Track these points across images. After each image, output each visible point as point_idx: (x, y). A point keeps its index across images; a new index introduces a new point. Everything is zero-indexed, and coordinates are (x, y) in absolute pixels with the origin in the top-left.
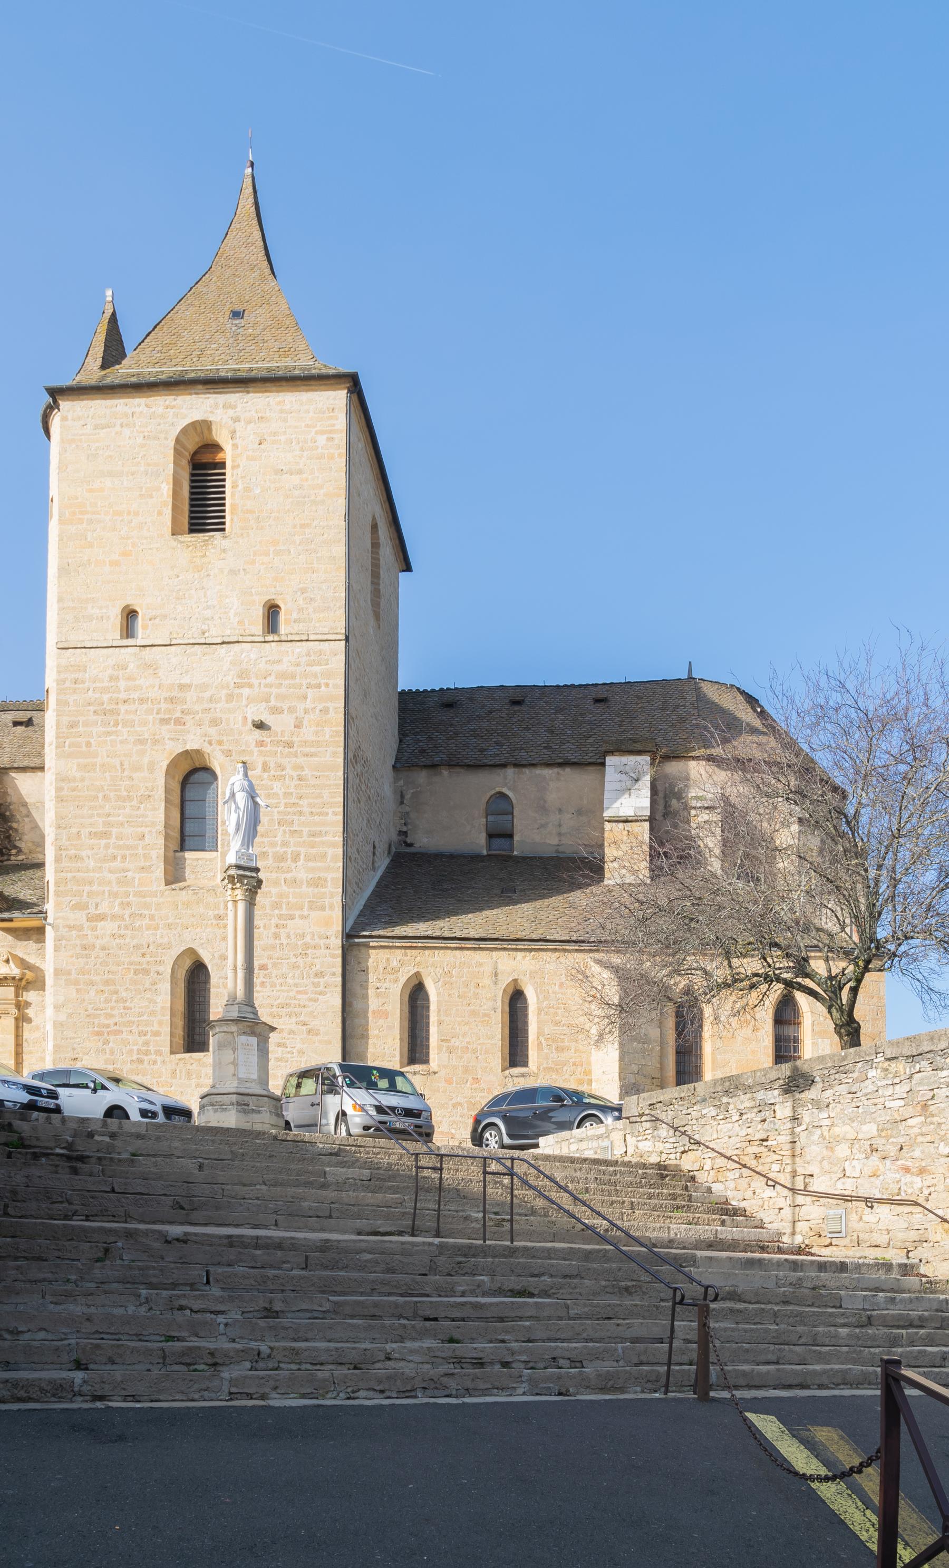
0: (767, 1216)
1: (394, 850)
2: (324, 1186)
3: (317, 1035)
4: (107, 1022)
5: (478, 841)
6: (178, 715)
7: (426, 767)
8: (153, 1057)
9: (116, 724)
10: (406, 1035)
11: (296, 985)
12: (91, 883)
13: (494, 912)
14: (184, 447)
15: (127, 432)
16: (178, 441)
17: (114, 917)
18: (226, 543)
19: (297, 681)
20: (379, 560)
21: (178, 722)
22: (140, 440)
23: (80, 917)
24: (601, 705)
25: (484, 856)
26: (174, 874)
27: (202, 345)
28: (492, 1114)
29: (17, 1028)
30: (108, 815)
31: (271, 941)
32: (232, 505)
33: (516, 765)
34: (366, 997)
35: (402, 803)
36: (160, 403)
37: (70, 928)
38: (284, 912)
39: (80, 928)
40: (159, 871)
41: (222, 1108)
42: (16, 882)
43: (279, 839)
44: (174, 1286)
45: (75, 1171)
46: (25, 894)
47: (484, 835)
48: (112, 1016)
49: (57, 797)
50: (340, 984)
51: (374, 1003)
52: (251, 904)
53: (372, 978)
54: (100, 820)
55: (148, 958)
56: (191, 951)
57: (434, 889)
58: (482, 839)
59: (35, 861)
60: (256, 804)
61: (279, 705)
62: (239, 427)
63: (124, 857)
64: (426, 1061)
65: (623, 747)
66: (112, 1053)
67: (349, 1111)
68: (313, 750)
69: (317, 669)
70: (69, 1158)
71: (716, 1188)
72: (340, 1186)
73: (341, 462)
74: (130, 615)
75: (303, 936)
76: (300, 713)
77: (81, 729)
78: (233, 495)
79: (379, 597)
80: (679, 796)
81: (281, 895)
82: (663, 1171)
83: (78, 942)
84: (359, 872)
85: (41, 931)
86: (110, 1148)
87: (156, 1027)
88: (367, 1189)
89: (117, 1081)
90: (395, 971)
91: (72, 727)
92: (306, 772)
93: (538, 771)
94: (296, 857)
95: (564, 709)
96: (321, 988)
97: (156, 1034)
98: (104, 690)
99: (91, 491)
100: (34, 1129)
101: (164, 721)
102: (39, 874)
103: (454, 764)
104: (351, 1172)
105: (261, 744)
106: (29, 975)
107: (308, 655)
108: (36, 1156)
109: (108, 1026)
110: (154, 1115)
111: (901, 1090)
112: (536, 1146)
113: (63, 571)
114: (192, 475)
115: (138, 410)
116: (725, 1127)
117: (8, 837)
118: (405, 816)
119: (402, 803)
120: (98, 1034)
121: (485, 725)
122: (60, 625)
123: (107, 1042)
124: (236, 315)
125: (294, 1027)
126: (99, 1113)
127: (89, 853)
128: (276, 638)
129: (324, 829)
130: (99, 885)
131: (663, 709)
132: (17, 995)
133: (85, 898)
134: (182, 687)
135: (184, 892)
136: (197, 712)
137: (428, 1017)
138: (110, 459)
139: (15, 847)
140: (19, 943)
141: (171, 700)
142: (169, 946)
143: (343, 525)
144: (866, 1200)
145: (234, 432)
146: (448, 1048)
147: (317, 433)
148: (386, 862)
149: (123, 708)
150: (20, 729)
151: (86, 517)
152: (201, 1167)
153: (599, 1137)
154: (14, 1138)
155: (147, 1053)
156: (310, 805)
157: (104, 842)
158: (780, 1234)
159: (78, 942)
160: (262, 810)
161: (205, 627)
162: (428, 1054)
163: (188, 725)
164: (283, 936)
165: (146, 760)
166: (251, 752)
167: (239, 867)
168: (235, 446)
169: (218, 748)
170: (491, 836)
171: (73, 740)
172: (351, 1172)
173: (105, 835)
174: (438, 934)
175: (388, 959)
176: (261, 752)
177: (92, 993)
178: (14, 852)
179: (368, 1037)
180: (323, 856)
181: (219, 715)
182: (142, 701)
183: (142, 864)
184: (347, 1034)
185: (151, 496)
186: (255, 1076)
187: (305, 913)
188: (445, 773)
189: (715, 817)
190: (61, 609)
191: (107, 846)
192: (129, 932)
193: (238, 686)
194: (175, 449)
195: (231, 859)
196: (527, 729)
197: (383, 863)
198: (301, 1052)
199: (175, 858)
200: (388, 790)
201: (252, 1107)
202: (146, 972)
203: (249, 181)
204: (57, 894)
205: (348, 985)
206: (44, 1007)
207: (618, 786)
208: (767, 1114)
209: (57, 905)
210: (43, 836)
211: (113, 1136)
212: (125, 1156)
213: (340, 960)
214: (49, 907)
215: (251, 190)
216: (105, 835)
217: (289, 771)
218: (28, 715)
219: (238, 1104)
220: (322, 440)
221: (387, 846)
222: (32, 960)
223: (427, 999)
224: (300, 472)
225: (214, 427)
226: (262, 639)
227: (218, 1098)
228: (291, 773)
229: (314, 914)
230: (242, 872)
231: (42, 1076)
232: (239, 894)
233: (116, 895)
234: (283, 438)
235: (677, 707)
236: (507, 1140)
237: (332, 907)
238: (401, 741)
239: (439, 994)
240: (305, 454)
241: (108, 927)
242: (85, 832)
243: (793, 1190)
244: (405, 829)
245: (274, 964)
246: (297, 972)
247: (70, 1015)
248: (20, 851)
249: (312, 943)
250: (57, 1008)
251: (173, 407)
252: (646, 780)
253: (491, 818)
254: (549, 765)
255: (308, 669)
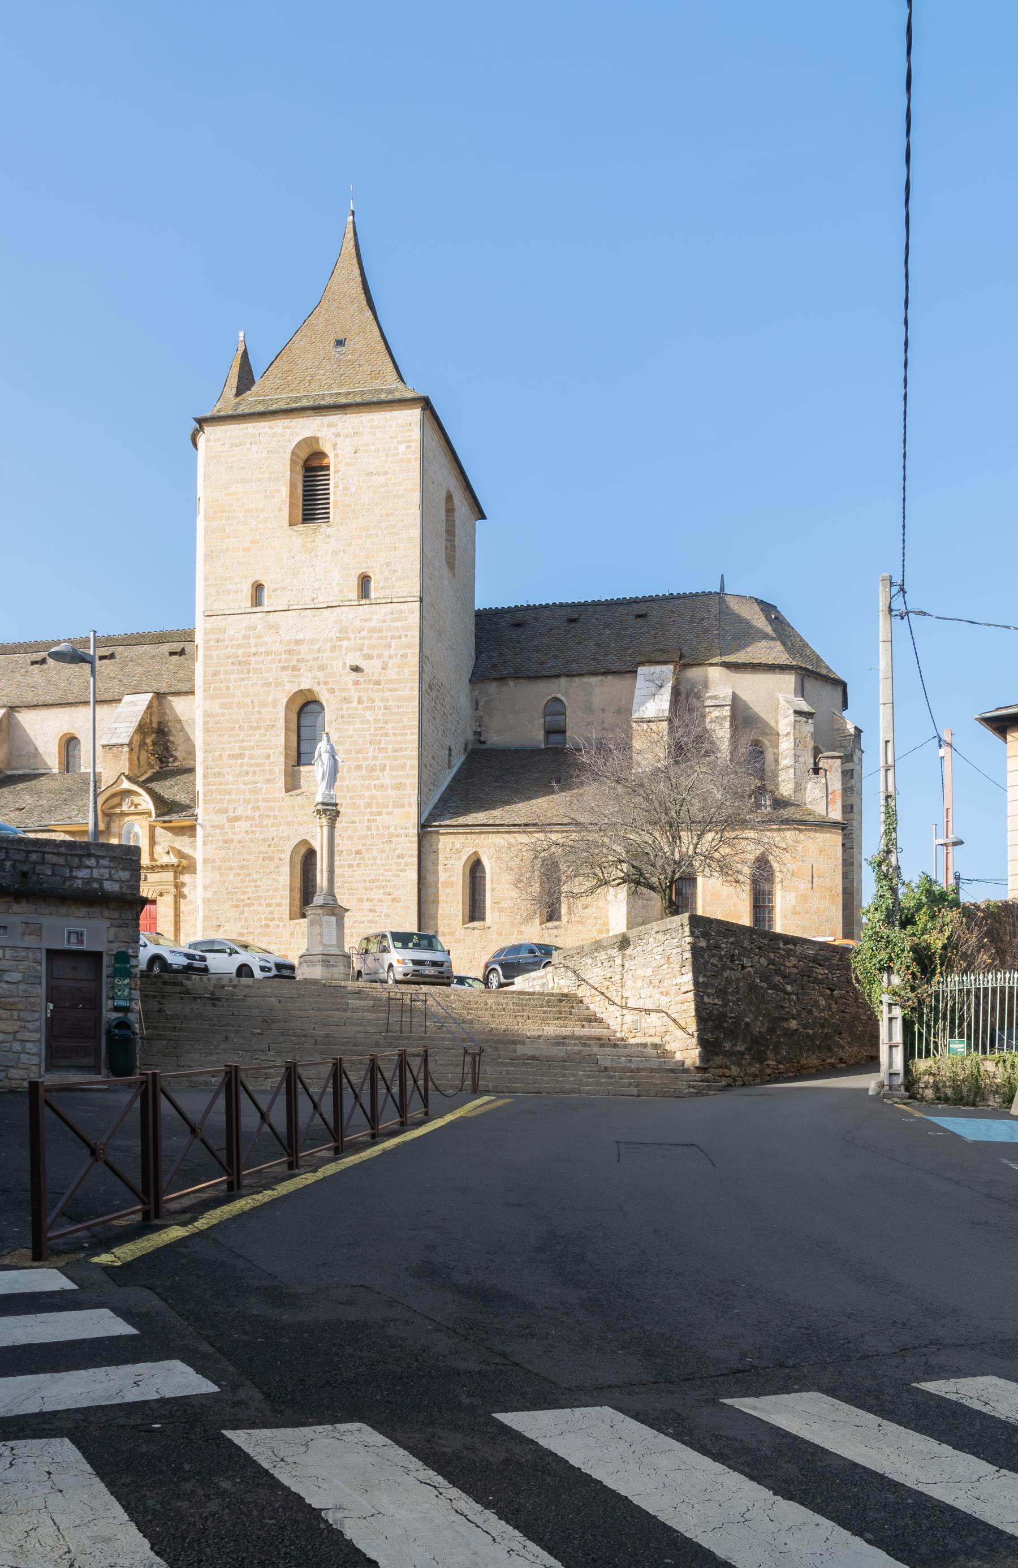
0: (611, 1022)
1: (470, 747)
2: (345, 1010)
3: (399, 902)
4: (242, 897)
5: (537, 737)
6: (294, 663)
7: (496, 679)
8: (277, 922)
9: (249, 672)
10: (468, 899)
11: (383, 865)
12: (230, 793)
13: (539, 800)
14: (298, 456)
15: (255, 448)
16: (293, 453)
17: (247, 818)
18: (330, 531)
19: (384, 633)
20: (454, 521)
21: (295, 668)
22: (265, 454)
23: (222, 819)
24: (641, 620)
25: (542, 750)
26: (292, 784)
27: (312, 371)
28: (494, 962)
29: (176, 902)
30: (243, 741)
31: (365, 832)
32: (335, 501)
33: (568, 676)
34: (436, 872)
35: (477, 709)
36: (279, 425)
37: (215, 827)
38: (374, 810)
39: (222, 827)
40: (281, 783)
41: (312, 964)
42: (173, 786)
43: (370, 755)
44: (255, 1051)
45: (214, 1005)
46: (181, 798)
47: (542, 732)
48: (246, 893)
49: (204, 729)
50: (416, 863)
51: (442, 876)
52: (332, 828)
53: (441, 857)
54: (237, 745)
55: (273, 848)
56: (305, 842)
57: (496, 781)
58: (541, 735)
59: (188, 766)
60: (335, 760)
61: (370, 652)
62: (339, 440)
63: (254, 773)
64: (483, 919)
65: (653, 658)
66: (246, 920)
67: (395, 964)
68: (395, 686)
69: (398, 624)
70: (212, 999)
71: (591, 1006)
72: (354, 1010)
73: (416, 465)
74: (258, 588)
75: (388, 828)
76: (386, 659)
77: (222, 676)
78: (335, 493)
79: (454, 551)
80: (698, 696)
81: (372, 797)
82: (564, 998)
83: (221, 838)
84: (435, 774)
85: (192, 829)
86: (233, 993)
87: (279, 900)
88: (369, 1011)
89: (246, 947)
90: (459, 851)
91: (215, 675)
92: (391, 703)
93: (585, 679)
94: (383, 768)
95: (609, 625)
96: (402, 867)
97: (279, 905)
98: (239, 647)
99: (228, 495)
100: (194, 984)
101: (285, 668)
102: (191, 778)
103: (519, 676)
104: (362, 1003)
105: (356, 683)
106: (184, 862)
107: (392, 613)
108: (195, 998)
109: (243, 900)
110: (269, 970)
111: (661, 949)
112: (513, 984)
113: (208, 557)
114: (305, 477)
115: (263, 431)
116: (596, 970)
117: (167, 748)
118: (479, 720)
119: (477, 709)
120: (236, 906)
121: (546, 641)
122: (206, 599)
123: (243, 912)
124: (340, 343)
125: (381, 897)
126: (233, 970)
127: (229, 770)
128: (368, 602)
129: (404, 746)
130: (236, 794)
131: (691, 622)
132: (175, 878)
133: (226, 805)
134: (298, 642)
135: (299, 798)
136: (309, 661)
137: (484, 885)
138: (244, 467)
139: (172, 756)
140: (177, 838)
141: (289, 652)
142: (289, 838)
143: (418, 512)
144: (646, 1010)
145: (335, 445)
146: (499, 908)
147: (398, 443)
148: (463, 758)
149: (253, 659)
150: (175, 658)
151: (225, 515)
152: (280, 1002)
153: (542, 977)
154: (184, 989)
155: (273, 919)
156: (393, 728)
157: (239, 761)
158: (616, 1032)
159: (221, 838)
160: (340, 764)
161: (314, 596)
162: (484, 914)
163: (302, 671)
164: (374, 828)
165: (270, 698)
166: (350, 689)
167: (323, 804)
168: (336, 456)
169: (324, 687)
170: (548, 732)
171: (216, 685)
172: (362, 1003)
173: (241, 756)
174: (491, 822)
175: (453, 843)
176: (357, 689)
177: (231, 876)
178: (171, 760)
179: (438, 903)
180: (404, 766)
181: (325, 662)
182: (267, 653)
183: (268, 777)
184: (422, 900)
185: (273, 497)
186: (334, 943)
187: (390, 810)
188: (511, 683)
189: (726, 712)
190: (206, 586)
191: (242, 765)
192: (258, 829)
193: (339, 639)
194: (291, 460)
195: (319, 799)
196: (580, 643)
197: (458, 761)
198: (387, 916)
199: (293, 771)
200: (464, 701)
201: (332, 963)
202: (271, 859)
203: (350, 227)
204: (205, 802)
205: (423, 863)
206: (195, 886)
207: (644, 692)
208: (612, 963)
209: (205, 810)
210: (193, 746)
211: (235, 987)
212: (241, 997)
213: (416, 845)
214: (199, 811)
215: (352, 234)
216: (241, 756)
217: (377, 703)
218: (181, 645)
219: (323, 961)
220: (402, 448)
221: (463, 746)
222: (186, 850)
223: (484, 872)
224: (385, 473)
225: (320, 441)
226: (357, 603)
227: (310, 958)
228: (379, 704)
229: (396, 811)
230: (326, 807)
231: (194, 945)
232: (324, 821)
233: (248, 801)
234: (372, 448)
235: (703, 619)
236: (503, 980)
237: (410, 805)
238: (477, 658)
239: (492, 868)
240: (389, 459)
241: (243, 826)
242: (225, 754)
243: (622, 1007)
244: (479, 730)
245: (367, 850)
246: (384, 855)
247: (215, 893)
248: (176, 759)
249: (395, 832)
250: (206, 888)
251: (290, 428)
252: (668, 687)
253: (548, 718)
254: (594, 674)
255: (392, 624)
